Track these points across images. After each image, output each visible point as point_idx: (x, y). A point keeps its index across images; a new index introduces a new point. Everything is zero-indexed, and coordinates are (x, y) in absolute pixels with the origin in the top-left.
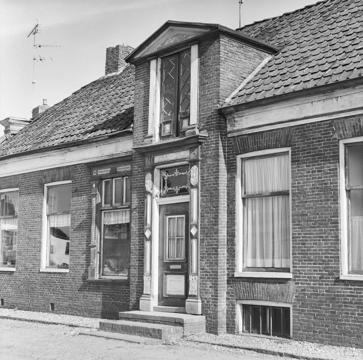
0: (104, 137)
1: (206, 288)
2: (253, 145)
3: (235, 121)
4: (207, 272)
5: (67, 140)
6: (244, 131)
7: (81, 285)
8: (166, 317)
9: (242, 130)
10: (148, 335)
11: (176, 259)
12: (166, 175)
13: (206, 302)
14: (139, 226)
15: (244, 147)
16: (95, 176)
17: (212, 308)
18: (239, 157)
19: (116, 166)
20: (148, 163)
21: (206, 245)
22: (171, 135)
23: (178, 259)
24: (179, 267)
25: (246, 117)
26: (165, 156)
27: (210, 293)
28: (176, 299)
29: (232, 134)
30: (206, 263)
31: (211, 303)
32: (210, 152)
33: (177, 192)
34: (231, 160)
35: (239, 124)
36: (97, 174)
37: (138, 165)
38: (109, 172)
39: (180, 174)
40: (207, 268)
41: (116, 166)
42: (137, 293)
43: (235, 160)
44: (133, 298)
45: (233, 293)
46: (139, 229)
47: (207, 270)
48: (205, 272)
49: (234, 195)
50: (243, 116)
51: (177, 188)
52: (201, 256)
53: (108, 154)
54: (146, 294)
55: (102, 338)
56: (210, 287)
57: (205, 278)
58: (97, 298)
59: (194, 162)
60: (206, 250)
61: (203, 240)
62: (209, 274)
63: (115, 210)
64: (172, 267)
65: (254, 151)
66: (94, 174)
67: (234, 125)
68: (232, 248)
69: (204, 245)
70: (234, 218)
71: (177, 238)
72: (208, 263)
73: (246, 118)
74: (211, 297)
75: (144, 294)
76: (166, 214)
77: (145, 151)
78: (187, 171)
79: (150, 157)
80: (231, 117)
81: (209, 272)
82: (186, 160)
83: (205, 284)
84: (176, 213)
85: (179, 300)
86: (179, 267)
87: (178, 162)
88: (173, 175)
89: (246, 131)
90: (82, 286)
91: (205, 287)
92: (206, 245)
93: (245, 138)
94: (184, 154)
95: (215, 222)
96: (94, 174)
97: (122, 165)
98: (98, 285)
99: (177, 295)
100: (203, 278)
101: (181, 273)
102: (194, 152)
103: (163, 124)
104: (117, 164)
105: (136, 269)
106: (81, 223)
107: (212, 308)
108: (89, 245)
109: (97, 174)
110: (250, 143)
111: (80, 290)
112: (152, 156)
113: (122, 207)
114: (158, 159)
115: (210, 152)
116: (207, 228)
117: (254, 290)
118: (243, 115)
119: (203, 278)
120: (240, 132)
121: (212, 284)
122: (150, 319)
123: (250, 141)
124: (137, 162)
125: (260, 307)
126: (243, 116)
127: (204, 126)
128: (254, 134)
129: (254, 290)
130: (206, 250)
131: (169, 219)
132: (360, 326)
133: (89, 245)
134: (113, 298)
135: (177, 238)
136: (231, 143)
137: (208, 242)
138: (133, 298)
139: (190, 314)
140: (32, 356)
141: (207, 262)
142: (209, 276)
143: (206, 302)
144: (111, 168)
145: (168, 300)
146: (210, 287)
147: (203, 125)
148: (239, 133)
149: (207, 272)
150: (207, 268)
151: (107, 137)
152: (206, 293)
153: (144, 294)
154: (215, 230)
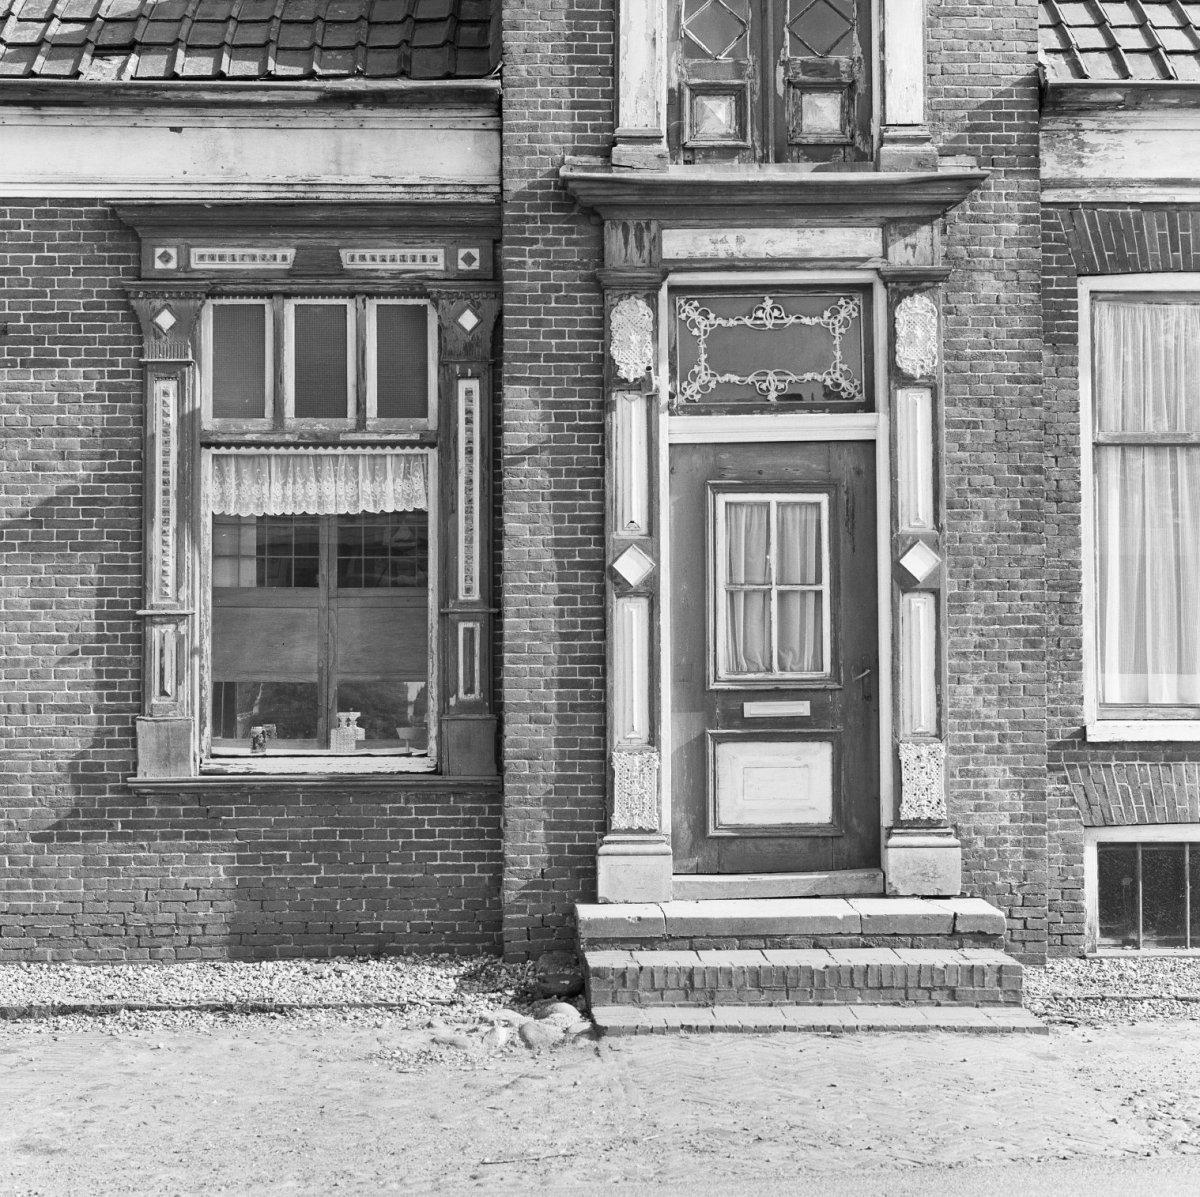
0: (290, 93)
1: (983, 791)
2: (1163, 245)
3: (1082, 145)
4: (984, 726)
5: (93, 77)
6: (1132, 191)
7: (65, 810)
8: (896, 916)
9: (1127, 183)
10: (936, 995)
11: (777, 674)
12: (699, 319)
13: (980, 844)
14: (558, 531)
15: (1121, 250)
16: (165, 276)
17: (1016, 866)
18: (1085, 285)
19: (337, 243)
20: (618, 246)
21: (977, 621)
22: (744, 148)
23: (788, 675)
24: (802, 708)
25: (1141, 136)
26: (731, 235)
27: (1002, 808)
28: (781, 841)
29: (1069, 191)
30: (978, 691)
31: (1008, 847)
32: (991, 250)
33: (772, 396)
34: (1056, 294)
35: (1106, 159)
36: (185, 265)
37: (541, 254)
38: (286, 266)
39: (792, 319)
40: (984, 711)
41: (337, 243)
42: (549, 826)
43: (1074, 294)
44: (530, 851)
45: (1073, 803)
46: (557, 542)
47: (987, 717)
48: (975, 726)
49: (1074, 431)
50: (1120, 131)
51: (771, 377)
52: (954, 662)
53: (281, 179)
54: (630, 831)
55: (781, 1034)
56: (1006, 785)
57: (974, 750)
58: (206, 872)
59: (905, 283)
60: (976, 638)
61: (960, 600)
62: (996, 733)
63: (321, 451)
64: (752, 709)
65: (1166, 270)
66: (159, 265)
67: (1080, 157)
68: (1068, 634)
69: (967, 621)
70: (1073, 518)
71: (782, 588)
72: (989, 691)
73: (1139, 143)
74: (1006, 822)
75: (617, 832)
76: (714, 486)
77: (635, 199)
78: (827, 314)
79: (639, 230)
80: (1065, 126)
81: (999, 726)
82: (862, 266)
83: (978, 775)
84: (777, 484)
85: (802, 845)
86: (802, 708)
87: (822, 269)
88: (748, 321)
89: (1143, 191)
90: (75, 813)
91: (976, 785)
92: (977, 621)
93: (1125, 216)
94: (857, 241)
95: (1023, 530)
96: (159, 265)
97: (386, 243)
98: (208, 805)
99: (789, 827)
100: (962, 751)
101: (811, 734)
102: (909, 240)
103: (687, 92)
104: (348, 233)
105: (545, 721)
106: (50, 501)
107: (1016, 866)
108: (140, 612)
109: (185, 265)
110: (1152, 242)
111: (59, 834)
112: (654, 226)
113: (358, 437)
114: (677, 243)
115: (991, 250)
116: (980, 552)
117: (1175, 787)
118: (1120, 127)
119: (962, 751)
120: (1110, 191)
121: (1014, 772)
122: (798, 930)
123: (1153, 230)
124: (535, 241)
125: (1187, 848)
126: (1120, 131)
127: (956, 140)
128: (1170, 208)
129: (1175, 787)
130: (976, 638)
131: (818, 505)
132: (8, 897)
133: (140, 612)
134: (329, 861)
135: (782, 588)
136: (1056, 227)
137: (989, 609)
138: (530, 851)
139: (914, 895)
140: (442, 1181)
141: (983, 686)
142: (997, 743)
143: (980, 844)
144: (298, 248)
145: (734, 847)
146: (1006, 785)
147: (954, 134)
148: (1108, 195)
149: (984, 726)
150: (984, 711)
151: (312, 96)
152: (978, 808)
153: (617, 832)
154: (1025, 563)
